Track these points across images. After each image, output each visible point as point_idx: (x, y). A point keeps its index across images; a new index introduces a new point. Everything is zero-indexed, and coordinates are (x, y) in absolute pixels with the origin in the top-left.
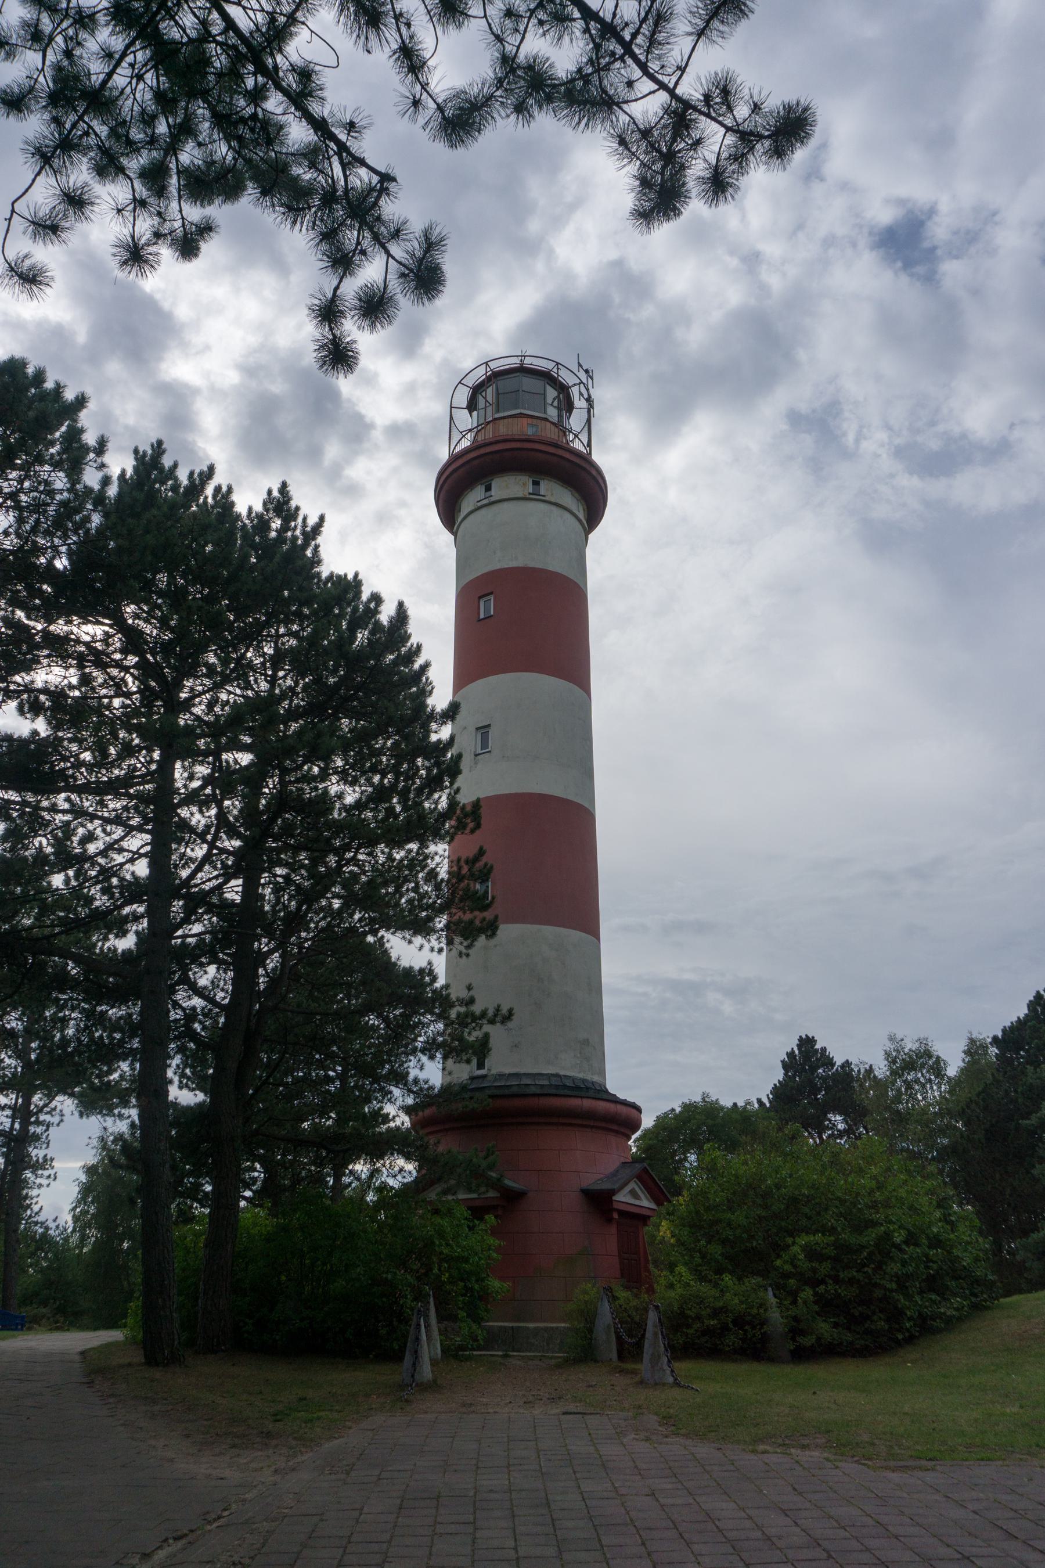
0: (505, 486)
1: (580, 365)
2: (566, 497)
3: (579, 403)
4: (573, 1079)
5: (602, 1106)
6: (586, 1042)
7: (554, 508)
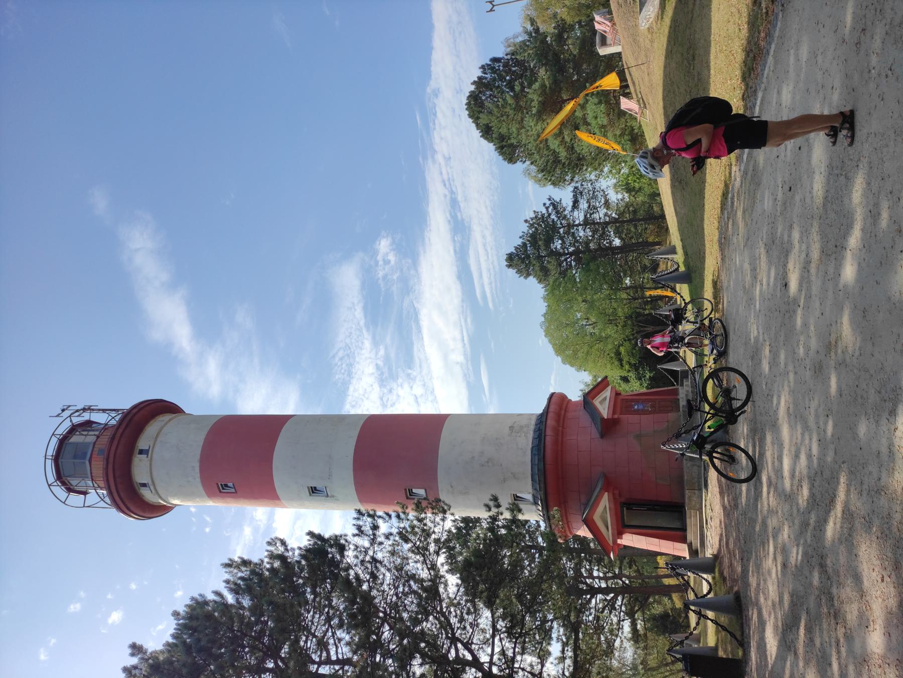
0: (140, 471)
1: (58, 416)
2: (151, 429)
3: (86, 416)
4: (534, 438)
5: (551, 422)
6: (511, 428)
7: (159, 439)
